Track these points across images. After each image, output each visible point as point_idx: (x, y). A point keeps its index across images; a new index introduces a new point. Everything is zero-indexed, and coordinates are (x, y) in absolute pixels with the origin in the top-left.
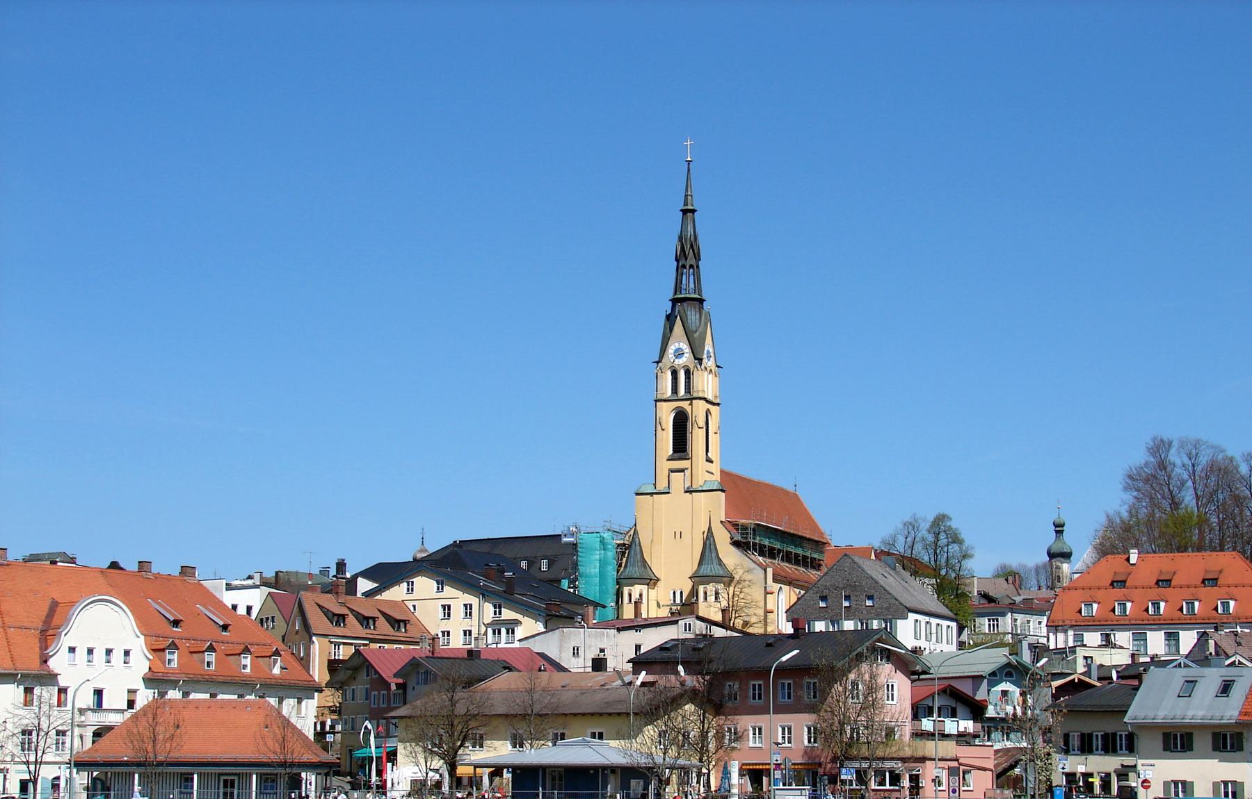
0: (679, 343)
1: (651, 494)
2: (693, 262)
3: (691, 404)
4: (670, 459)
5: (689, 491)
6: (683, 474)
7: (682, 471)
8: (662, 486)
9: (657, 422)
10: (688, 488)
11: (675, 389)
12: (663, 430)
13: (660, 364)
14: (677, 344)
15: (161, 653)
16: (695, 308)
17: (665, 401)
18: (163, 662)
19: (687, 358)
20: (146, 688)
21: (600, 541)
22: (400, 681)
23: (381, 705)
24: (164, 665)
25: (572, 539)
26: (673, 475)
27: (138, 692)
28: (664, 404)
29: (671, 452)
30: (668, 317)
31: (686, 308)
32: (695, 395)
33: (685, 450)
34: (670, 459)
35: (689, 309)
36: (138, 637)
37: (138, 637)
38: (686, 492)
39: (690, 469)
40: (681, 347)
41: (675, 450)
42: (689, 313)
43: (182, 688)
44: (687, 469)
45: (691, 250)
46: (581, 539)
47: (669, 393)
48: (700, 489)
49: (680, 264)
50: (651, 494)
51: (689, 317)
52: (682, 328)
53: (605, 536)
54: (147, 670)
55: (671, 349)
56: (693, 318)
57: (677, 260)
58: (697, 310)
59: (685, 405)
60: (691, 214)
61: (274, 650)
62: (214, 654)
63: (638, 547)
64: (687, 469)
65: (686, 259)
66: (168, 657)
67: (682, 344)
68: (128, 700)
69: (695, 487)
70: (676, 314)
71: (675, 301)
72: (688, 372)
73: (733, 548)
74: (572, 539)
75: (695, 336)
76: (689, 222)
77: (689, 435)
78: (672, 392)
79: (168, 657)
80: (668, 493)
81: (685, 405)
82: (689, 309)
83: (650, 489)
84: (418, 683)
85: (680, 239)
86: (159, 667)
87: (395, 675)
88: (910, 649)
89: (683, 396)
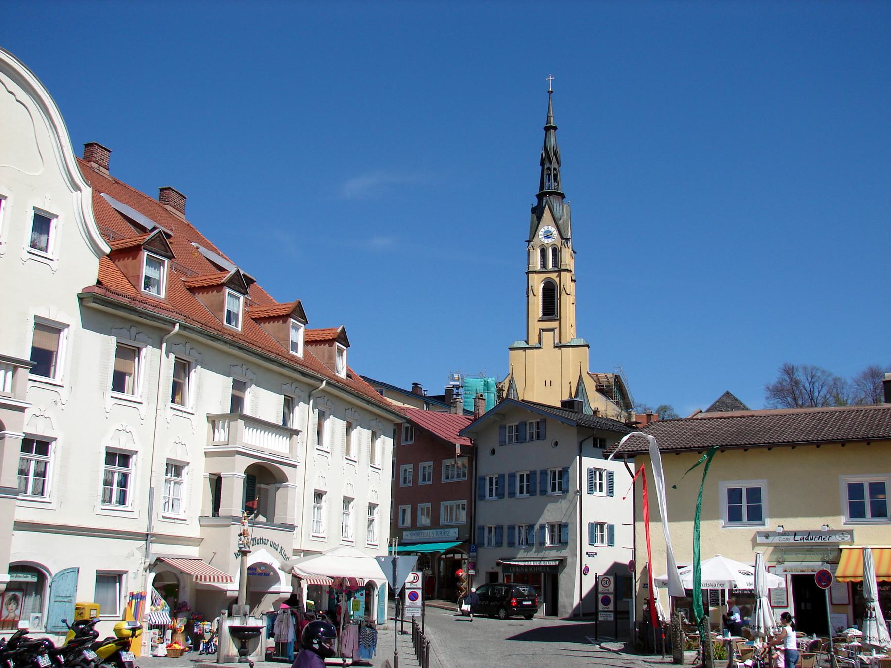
0: (547, 226)
1: (524, 349)
2: (556, 166)
3: (559, 276)
4: (541, 320)
5: (559, 347)
6: (552, 332)
7: (553, 330)
8: (533, 341)
9: (528, 291)
10: (557, 344)
11: (544, 263)
12: (534, 296)
13: (531, 243)
14: (546, 227)
15: (129, 262)
16: (559, 200)
17: (536, 272)
18: (133, 279)
19: (555, 239)
20: (83, 327)
21: (484, 385)
22: (467, 443)
23: (420, 482)
24: (135, 287)
25: (458, 383)
26: (543, 333)
27: (63, 334)
28: (535, 275)
29: (540, 315)
30: (534, 210)
31: (552, 200)
32: (563, 267)
33: (552, 313)
34: (541, 320)
35: (555, 201)
36: (77, 188)
37: (77, 188)
38: (555, 347)
39: (558, 329)
40: (550, 229)
41: (544, 313)
42: (555, 204)
43: (175, 348)
44: (556, 328)
45: (554, 157)
46: (466, 383)
47: (538, 267)
48: (569, 344)
49: (546, 167)
50: (524, 349)
51: (555, 207)
52: (550, 214)
53: (489, 380)
54: (94, 283)
55: (541, 232)
56: (558, 208)
57: (542, 164)
58: (561, 203)
59: (554, 276)
60: (554, 130)
61: (339, 330)
62: (242, 298)
63: (515, 392)
64: (556, 328)
65: (551, 162)
66: (146, 270)
67: (550, 227)
68: (33, 348)
69: (563, 343)
70: (544, 204)
71: (540, 197)
72: (555, 251)
73: (598, 395)
74: (458, 383)
75: (560, 222)
76: (552, 136)
77: (557, 302)
78: (541, 267)
79: (146, 270)
80: (540, 348)
81: (554, 276)
82: (555, 201)
83: (524, 345)
84: (502, 443)
85: (545, 148)
86: (119, 283)
87: (462, 433)
88: (16, 605)
89: (551, 269)
